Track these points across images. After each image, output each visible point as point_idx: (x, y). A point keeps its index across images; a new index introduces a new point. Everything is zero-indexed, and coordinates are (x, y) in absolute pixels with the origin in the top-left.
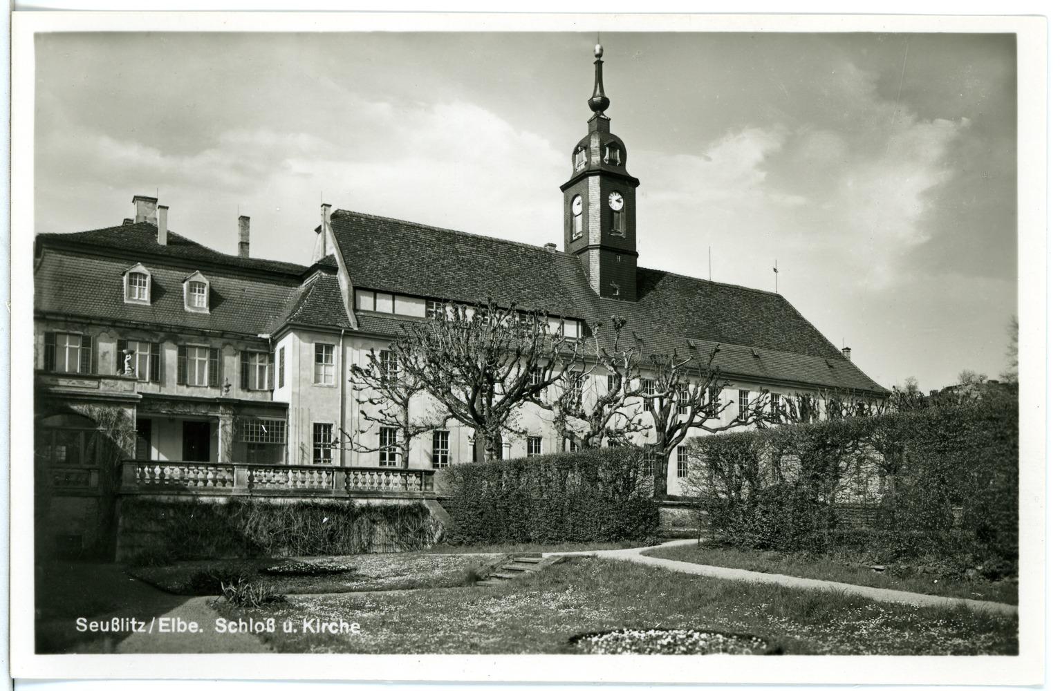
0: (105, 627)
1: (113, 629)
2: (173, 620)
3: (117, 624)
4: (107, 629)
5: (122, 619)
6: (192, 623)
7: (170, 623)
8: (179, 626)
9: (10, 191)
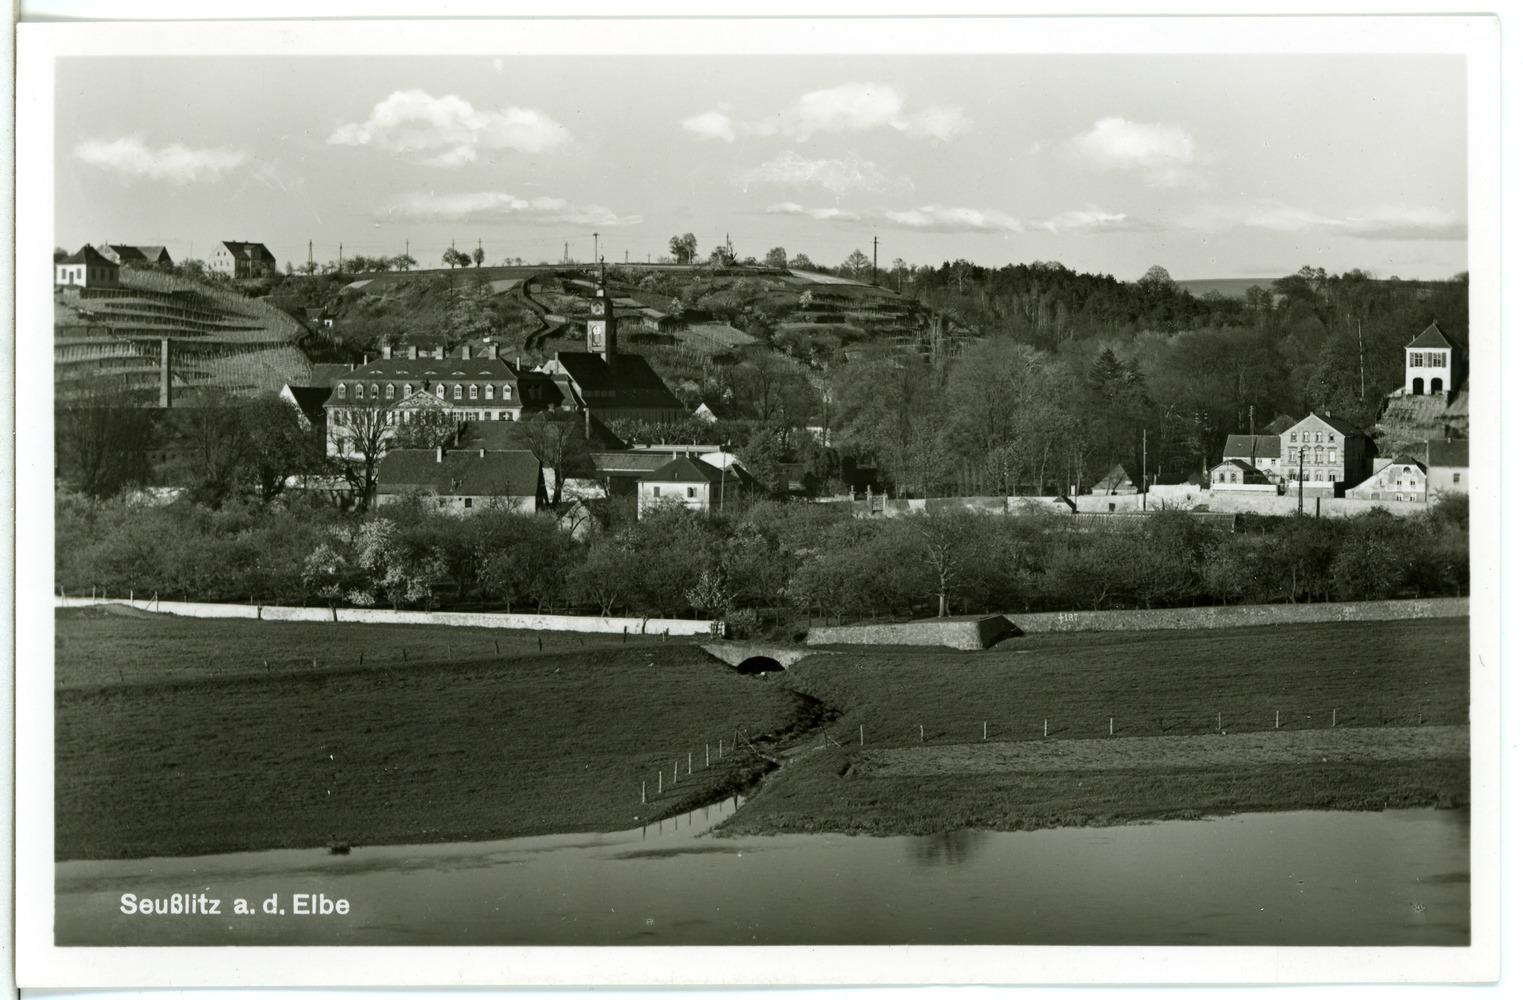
0: (161, 908)
1: (174, 911)
2: (314, 897)
3: (179, 902)
4: (165, 911)
5: (187, 896)
6: (144, 901)
7: (309, 901)
8: (322, 907)
9: (15, 373)
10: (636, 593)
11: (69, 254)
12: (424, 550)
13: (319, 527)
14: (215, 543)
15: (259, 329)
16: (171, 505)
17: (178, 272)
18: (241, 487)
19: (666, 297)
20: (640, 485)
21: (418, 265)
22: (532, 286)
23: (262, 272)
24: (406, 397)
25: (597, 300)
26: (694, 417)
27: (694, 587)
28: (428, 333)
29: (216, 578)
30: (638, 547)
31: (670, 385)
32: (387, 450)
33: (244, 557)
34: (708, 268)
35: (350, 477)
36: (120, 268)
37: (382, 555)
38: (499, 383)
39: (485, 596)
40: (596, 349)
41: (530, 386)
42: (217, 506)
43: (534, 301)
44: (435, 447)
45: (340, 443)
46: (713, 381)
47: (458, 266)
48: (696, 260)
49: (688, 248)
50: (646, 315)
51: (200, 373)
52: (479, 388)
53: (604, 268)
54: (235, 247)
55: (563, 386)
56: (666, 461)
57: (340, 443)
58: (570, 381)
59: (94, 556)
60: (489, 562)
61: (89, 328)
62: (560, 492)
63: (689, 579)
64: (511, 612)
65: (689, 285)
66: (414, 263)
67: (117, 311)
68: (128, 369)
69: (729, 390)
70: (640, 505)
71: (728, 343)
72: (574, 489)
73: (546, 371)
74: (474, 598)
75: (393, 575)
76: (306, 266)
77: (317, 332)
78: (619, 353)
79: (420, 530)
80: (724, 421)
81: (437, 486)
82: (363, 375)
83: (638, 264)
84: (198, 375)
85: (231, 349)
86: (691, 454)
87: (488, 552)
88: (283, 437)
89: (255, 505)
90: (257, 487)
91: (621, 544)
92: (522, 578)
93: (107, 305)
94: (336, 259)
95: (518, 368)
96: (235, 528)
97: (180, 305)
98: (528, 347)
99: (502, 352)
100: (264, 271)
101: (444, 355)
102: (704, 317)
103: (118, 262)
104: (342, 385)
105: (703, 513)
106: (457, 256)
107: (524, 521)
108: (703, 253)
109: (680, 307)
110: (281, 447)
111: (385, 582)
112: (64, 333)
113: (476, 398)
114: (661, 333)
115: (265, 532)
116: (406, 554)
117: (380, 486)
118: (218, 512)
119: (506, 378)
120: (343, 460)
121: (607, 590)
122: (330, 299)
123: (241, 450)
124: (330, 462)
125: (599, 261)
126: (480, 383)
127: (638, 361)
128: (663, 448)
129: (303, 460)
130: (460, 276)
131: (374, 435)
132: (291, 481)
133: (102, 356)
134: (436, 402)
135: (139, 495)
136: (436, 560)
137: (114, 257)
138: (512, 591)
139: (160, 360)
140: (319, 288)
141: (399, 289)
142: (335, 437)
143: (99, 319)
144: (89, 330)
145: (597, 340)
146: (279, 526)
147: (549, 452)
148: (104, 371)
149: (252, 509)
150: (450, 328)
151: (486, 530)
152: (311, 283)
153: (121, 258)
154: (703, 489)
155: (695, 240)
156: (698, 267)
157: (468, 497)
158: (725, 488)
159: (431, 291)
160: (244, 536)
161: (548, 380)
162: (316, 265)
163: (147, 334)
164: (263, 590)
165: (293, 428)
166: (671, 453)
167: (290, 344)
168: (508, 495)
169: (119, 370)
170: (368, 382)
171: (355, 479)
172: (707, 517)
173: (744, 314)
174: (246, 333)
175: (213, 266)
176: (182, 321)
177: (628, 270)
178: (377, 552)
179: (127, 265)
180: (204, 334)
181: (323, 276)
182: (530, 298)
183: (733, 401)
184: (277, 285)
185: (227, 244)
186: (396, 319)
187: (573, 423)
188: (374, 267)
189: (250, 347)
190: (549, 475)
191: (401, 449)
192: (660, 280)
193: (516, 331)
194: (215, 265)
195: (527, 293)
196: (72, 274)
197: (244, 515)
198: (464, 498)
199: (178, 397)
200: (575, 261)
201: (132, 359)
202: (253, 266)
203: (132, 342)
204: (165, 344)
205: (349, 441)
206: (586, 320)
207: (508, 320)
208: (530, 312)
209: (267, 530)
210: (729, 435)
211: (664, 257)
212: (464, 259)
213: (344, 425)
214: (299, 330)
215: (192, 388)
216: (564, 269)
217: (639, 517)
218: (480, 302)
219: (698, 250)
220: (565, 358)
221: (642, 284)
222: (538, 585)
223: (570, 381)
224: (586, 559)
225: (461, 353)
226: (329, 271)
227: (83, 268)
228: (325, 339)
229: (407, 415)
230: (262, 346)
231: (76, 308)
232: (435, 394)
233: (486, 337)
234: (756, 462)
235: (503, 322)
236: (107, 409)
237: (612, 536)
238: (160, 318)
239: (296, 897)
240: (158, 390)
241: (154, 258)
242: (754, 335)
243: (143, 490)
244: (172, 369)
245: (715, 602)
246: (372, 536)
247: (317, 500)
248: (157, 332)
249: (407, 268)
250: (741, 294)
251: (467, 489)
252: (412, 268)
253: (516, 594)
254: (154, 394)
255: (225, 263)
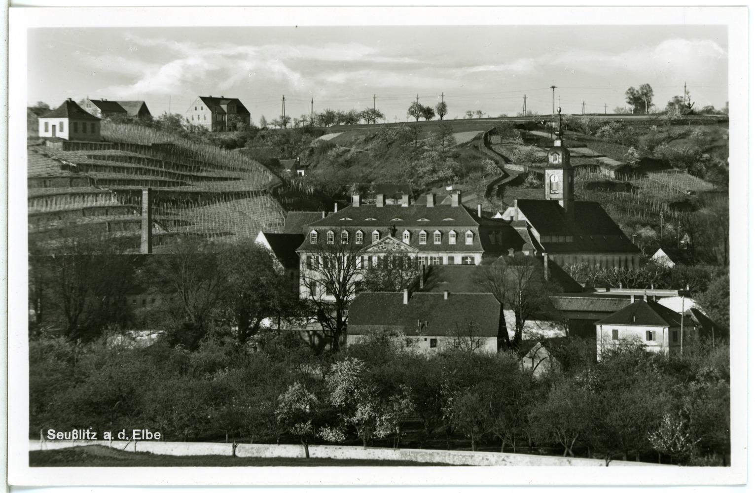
0: (68, 437)
2: (143, 431)
3: (76, 434)
5: (80, 431)
6: (59, 433)
10: (597, 434)
11: (51, 108)
12: (392, 388)
13: (292, 366)
14: (193, 383)
15: (235, 179)
16: (150, 346)
17: (157, 126)
18: (217, 329)
19: (623, 146)
20: (598, 327)
21: (384, 119)
22: (492, 137)
23: (238, 126)
24: (374, 243)
25: (555, 150)
26: (652, 262)
27: (657, 429)
28: (394, 182)
29: (193, 417)
30: (599, 388)
31: (627, 231)
32: (356, 292)
33: (219, 396)
34: (665, 117)
35: (322, 318)
36: (101, 122)
37: (352, 393)
38: (461, 229)
39: (449, 433)
40: (554, 197)
41: (490, 233)
42: (194, 347)
43: (494, 152)
44: (401, 289)
45: (312, 286)
46: (670, 227)
47: (422, 119)
48: (652, 110)
49: (644, 98)
50: (602, 164)
51: (178, 221)
52: (442, 234)
53: (561, 120)
54: (211, 102)
55: (523, 231)
56: (624, 305)
57: (312, 286)
58: (529, 227)
59: (74, 398)
60: (454, 400)
61: (72, 178)
62: (520, 333)
63: (651, 422)
64: (476, 450)
65: (646, 134)
66: (380, 116)
67: (99, 162)
68: (110, 218)
69: (686, 236)
70: (599, 347)
71: (686, 190)
72: (534, 331)
73: (506, 217)
74: (441, 436)
75: (362, 413)
76: (279, 119)
77: (290, 181)
78: (577, 200)
79: (388, 369)
80: (682, 267)
81: (403, 327)
82: (334, 222)
83: (594, 115)
84: (177, 223)
85: (210, 198)
86: (649, 298)
87: (453, 390)
88: (258, 279)
89: (230, 346)
90: (233, 328)
91: (580, 384)
92: (486, 416)
93: (90, 157)
94: (307, 112)
95: (479, 215)
96: (212, 367)
97: (160, 157)
98: (488, 194)
99: (464, 200)
100: (240, 125)
101: (410, 203)
102: (662, 165)
103: (99, 115)
104: (314, 232)
105: (663, 356)
106: (421, 109)
107: (486, 361)
108: (659, 103)
109: (636, 155)
110: (256, 290)
111: (355, 419)
112: (48, 183)
113: (440, 243)
114: (617, 181)
115: (240, 372)
116: (374, 392)
117: (350, 327)
118: (196, 353)
119: (468, 224)
120: (314, 302)
121: (568, 431)
122: (302, 150)
123: (218, 293)
124: (303, 304)
125: (556, 113)
126: (444, 229)
127: (595, 207)
128: (620, 291)
129: (277, 302)
130: (424, 129)
131: (344, 278)
132: (266, 322)
133: (85, 206)
134: (402, 248)
135: (120, 338)
136: (403, 397)
137: (96, 111)
138: (476, 429)
139: (141, 208)
140: (292, 141)
141: (367, 141)
142: (308, 280)
143: (81, 170)
144: (72, 181)
145: (554, 188)
146: (253, 366)
147: (509, 294)
148: (87, 220)
149: (228, 350)
150: (415, 177)
151: (451, 369)
152: (284, 136)
153: (102, 112)
154: (662, 332)
155: (651, 91)
156: (655, 117)
157: (434, 337)
158: (684, 332)
159: (397, 143)
160: (221, 376)
161: (507, 226)
162: (289, 119)
163: (128, 185)
164: (238, 428)
165: (268, 272)
166: (629, 297)
167: (265, 192)
168: (471, 336)
169: (102, 219)
170: (338, 228)
171: (327, 320)
172: (667, 360)
173: (702, 161)
174: (222, 183)
175: (190, 120)
176: (162, 172)
177: (585, 121)
178: (347, 390)
179: (108, 119)
180: (182, 184)
181: (295, 129)
182: (491, 149)
183: (691, 247)
184: (252, 138)
185: (205, 100)
186: (364, 169)
187: (532, 267)
188: (343, 121)
189: (226, 196)
190: (510, 317)
191: (370, 292)
192: (616, 130)
193: (478, 180)
194: (193, 119)
195: (488, 144)
196: (54, 126)
197: (220, 355)
198: (429, 338)
199: (158, 244)
200: (533, 113)
201: (114, 207)
202: (229, 120)
203: (113, 192)
204: (145, 193)
205: (321, 284)
206: (544, 168)
207: (470, 169)
208: (490, 161)
209: (243, 369)
210: (687, 280)
211: (621, 107)
212: (428, 113)
213: (316, 269)
214: (273, 179)
215: (172, 235)
216: (523, 121)
217: (599, 359)
218: (443, 152)
219: (654, 100)
220: (524, 205)
221: (599, 134)
222: (501, 422)
223: (529, 227)
224: (547, 398)
225: (426, 201)
226: (301, 125)
227: (66, 121)
228: (297, 188)
229: (375, 259)
230: (239, 195)
231: (58, 160)
232: (401, 240)
233: (448, 185)
234: (717, 307)
235: (464, 171)
236: (90, 256)
237: (571, 376)
238: (141, 169)
239: (134, 431)
240: (140, 237)
241: (134, 112)
242: (713, 182)
243: (123, 334)
244: (153, 217)
245: (679, 445)
246: (343, 374)
247: (292, 340)
248: (139, 182)
249: (375, 121)
250: (697, 141)
251: (432, 330)
252: (379, 121)
253: (480, 432)
254: (135, 242)
255: (202, 117)
